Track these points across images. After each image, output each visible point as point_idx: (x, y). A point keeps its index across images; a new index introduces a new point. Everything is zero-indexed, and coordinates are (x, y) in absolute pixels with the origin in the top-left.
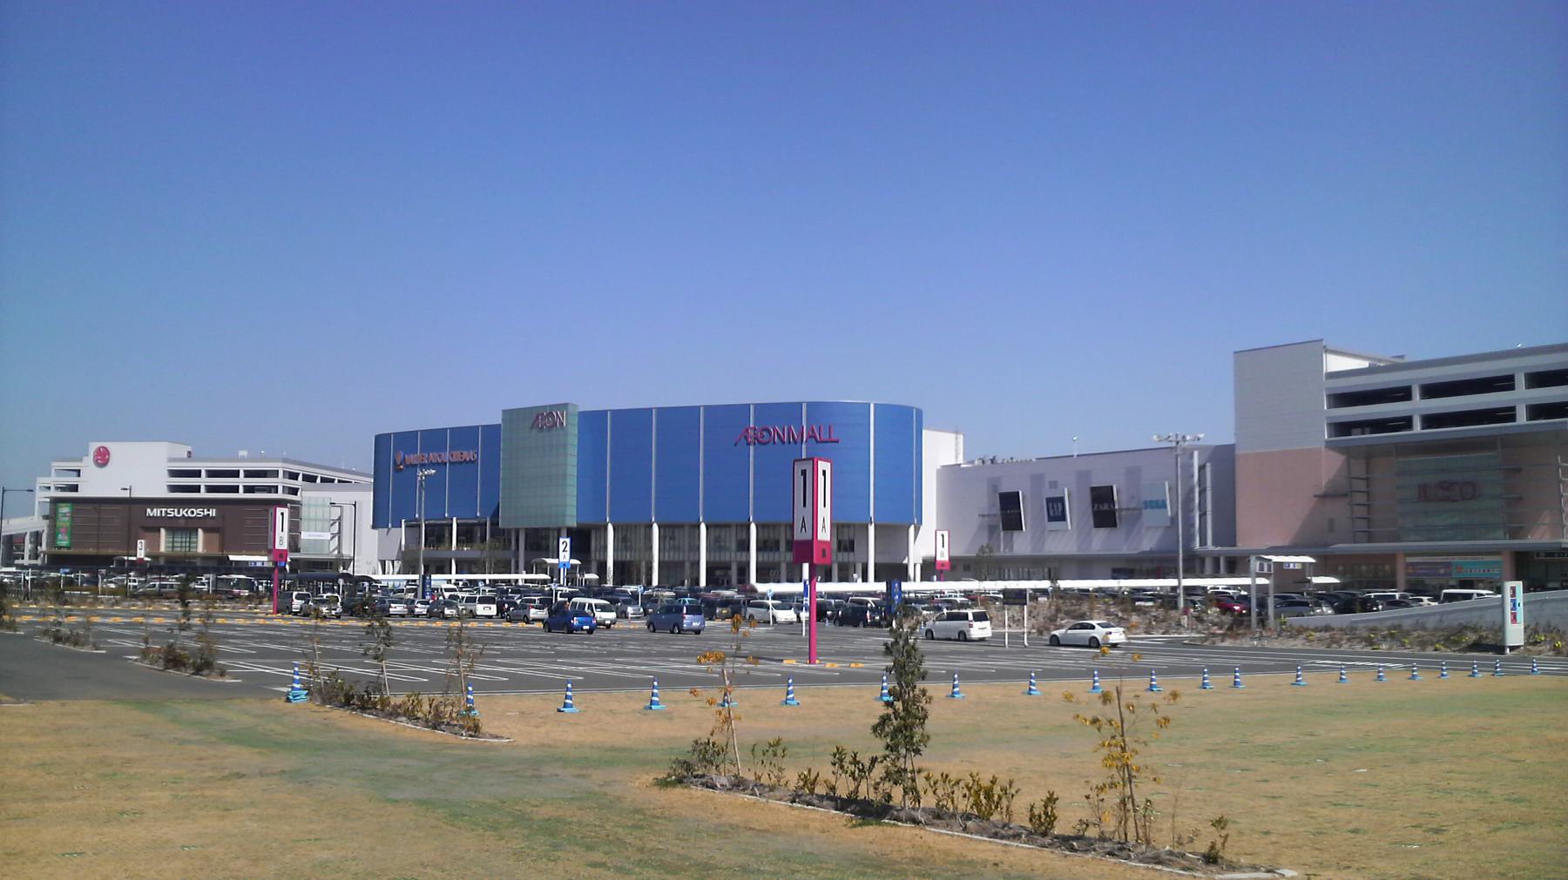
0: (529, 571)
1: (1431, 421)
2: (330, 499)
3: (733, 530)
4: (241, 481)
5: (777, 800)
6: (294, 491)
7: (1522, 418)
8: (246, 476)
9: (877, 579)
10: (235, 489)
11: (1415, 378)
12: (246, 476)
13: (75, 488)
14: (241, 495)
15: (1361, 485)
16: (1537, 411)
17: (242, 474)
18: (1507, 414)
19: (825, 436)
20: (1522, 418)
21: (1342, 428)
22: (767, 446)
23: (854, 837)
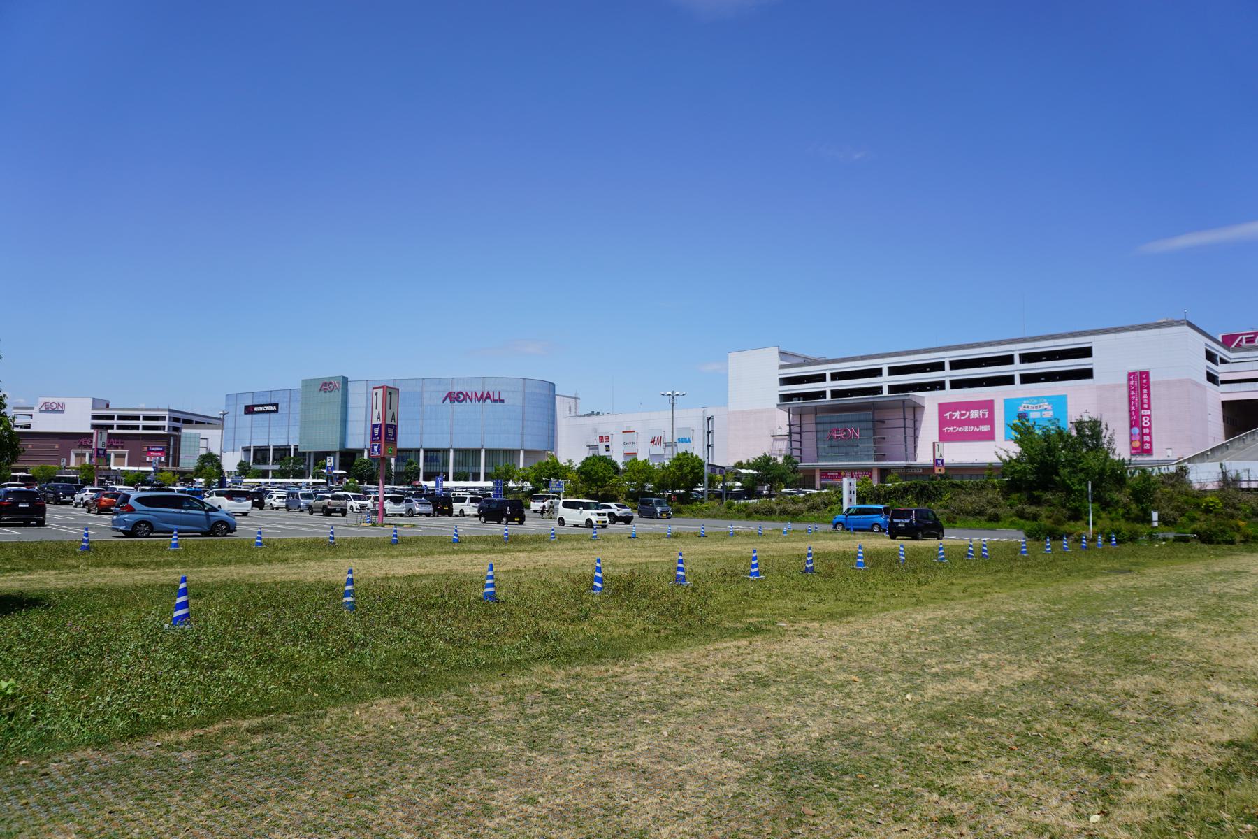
0: (314, 478)
1: (835, 394)
2: (595, 431)
3: (414, 452)
4: (116, 422)
5: (204, 534)
6: (176, 429)
7: (885, 392)
8: (952, 368)
9: (486, 479)
10: (137, 427)
11: (142, 414)
12: (952, 368)
13: (28, 426)
14: (141, 431)
15: (797, 429)
16: (893, 389)
17: (1017, 359)
18: (878, 390)
19: (496, 398)
20: (885, 392)
21: (786, 398)
22: (442, 400)
23: (975, 686)
